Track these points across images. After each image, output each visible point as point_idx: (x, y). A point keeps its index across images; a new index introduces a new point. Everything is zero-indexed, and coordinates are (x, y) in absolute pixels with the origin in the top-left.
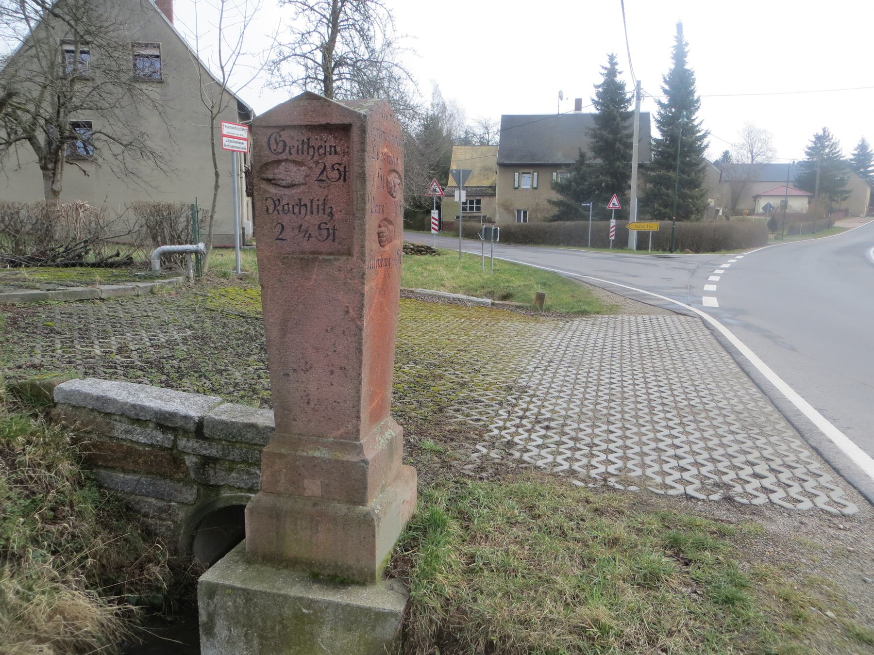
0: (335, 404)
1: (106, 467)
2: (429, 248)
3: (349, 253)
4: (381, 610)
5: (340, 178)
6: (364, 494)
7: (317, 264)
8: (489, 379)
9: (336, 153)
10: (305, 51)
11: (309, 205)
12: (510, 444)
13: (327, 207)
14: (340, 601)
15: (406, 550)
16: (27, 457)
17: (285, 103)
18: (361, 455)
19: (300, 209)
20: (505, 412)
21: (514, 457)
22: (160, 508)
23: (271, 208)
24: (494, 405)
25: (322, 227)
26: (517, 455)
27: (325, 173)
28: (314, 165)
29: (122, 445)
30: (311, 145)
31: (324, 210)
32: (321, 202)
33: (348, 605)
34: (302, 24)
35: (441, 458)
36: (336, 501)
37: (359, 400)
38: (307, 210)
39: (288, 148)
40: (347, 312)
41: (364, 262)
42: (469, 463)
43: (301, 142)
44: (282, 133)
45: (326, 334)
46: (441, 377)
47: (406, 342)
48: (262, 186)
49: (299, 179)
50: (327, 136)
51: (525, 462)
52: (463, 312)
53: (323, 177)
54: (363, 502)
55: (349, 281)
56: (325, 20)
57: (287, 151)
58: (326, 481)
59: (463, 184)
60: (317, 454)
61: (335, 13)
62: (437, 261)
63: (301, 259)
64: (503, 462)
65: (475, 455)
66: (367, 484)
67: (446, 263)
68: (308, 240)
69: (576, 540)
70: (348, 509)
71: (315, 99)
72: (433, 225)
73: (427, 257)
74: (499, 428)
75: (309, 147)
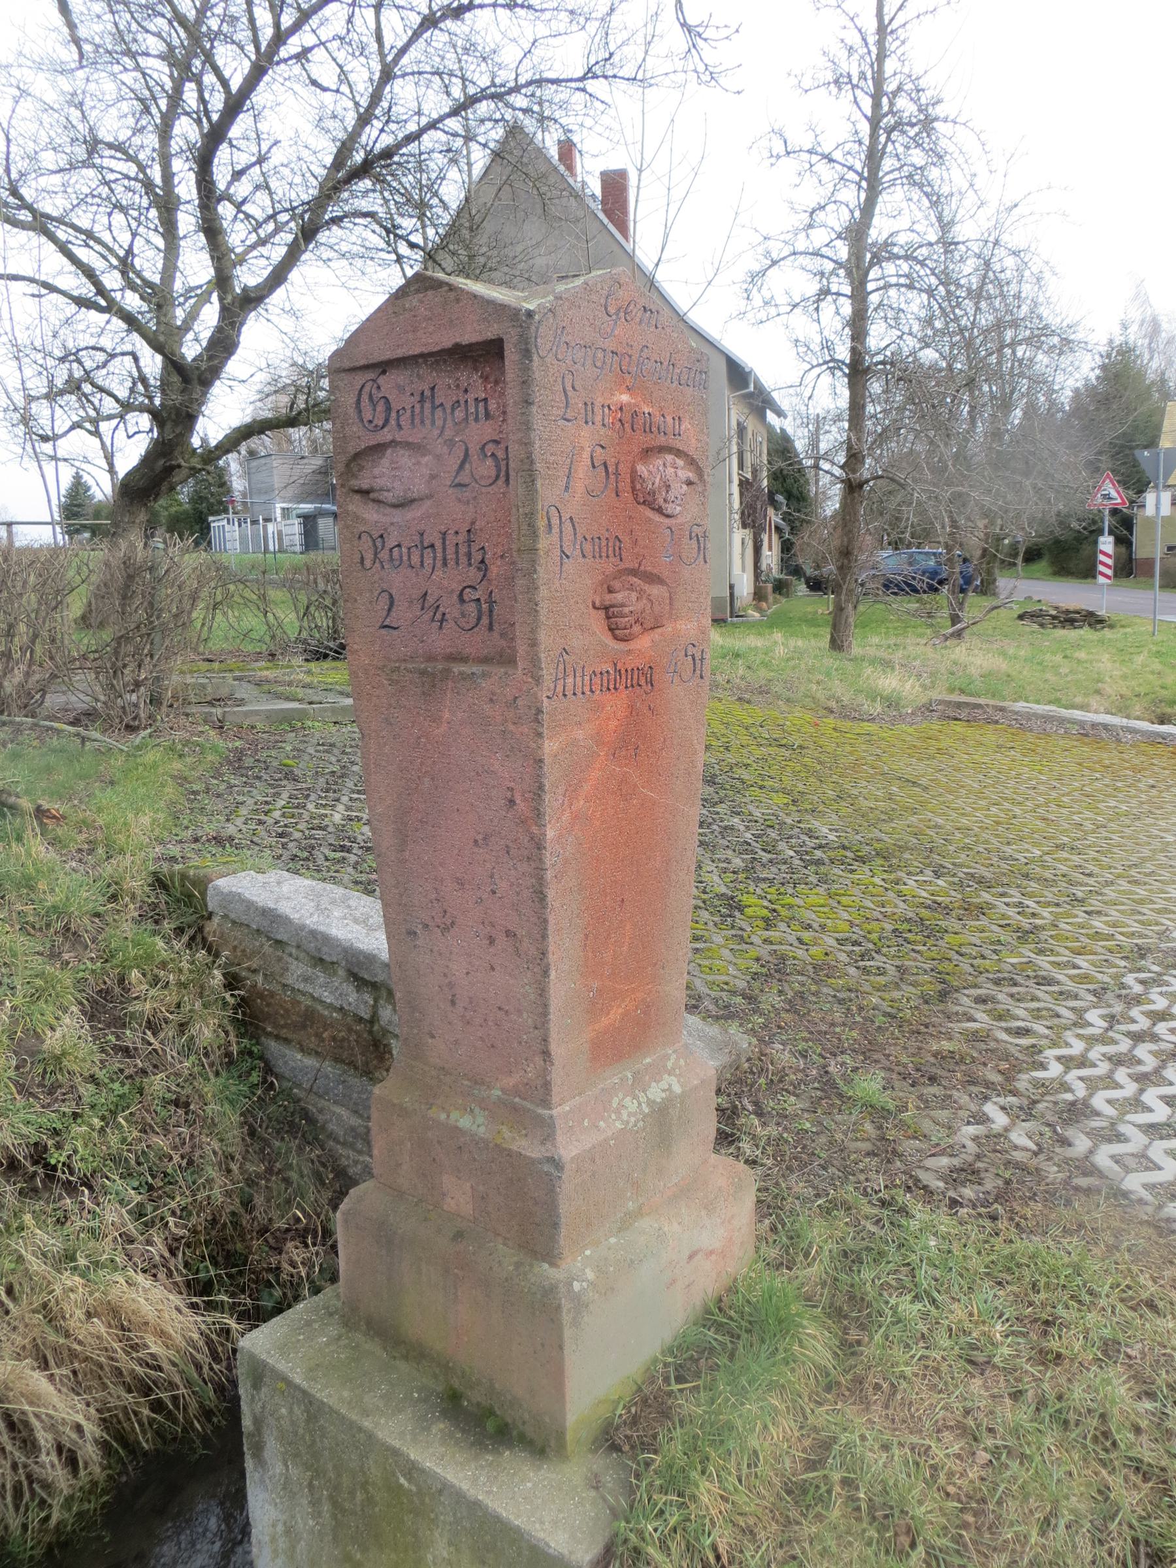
0: (500, 1014)
1: (277, 1037)
2: (1091, 614)
3: (511, 661)
4: (542, 1545)
5: (497, 477)
6: (553, 1238)
7: (450, 684)
8: (1098, 924)
9: (488, 416)
10: (817, 245)
11: (438, 545)
12: (1077, 1112)
13: (475, 547)
14: (465, 1486)
15: (680, 1379)
16: (148, 1006)
17: (379, 310)
18: (549, 1145)
19: (422, 556)
20: (1102, 1017)
21: (1070, 1152)
22: (353, 1129)
23: (369, 557)
24: (1082, 993)
25: (466, 597)
26: (1082, 1144)
27: (467, 466)
28: (445, 450)
29: (299, 1002)
30: (437, 403)
31: (469, 555)
32: (462, 538)
33: (476, 1504)
34: (811, 195)
35: (880, 1128)
36: (500, 1240)
37: (545, 1014)
38: (435, 558)
39: (394, 415)
40: (512, 802)
41: (538, 680)
42: (943, 1153)
43: (418, 398)
44: (381, 380)
45: (476, 850)
46: (982, 910)
47: (940, 821)
48: (351, 507)
49: (419, 487)
50: (469, 378)
51: (1091, 1170)
52: (1105, 756)
53: (464, 478)
54: (550, 1256)
55: (511, 727)
56: (851, 176)
57: (393, 422)
58: (481, 1188)
59: (1167, 477)
60: (465, 1122)
61: (874, 157)
62: (1101, 642)
63: (423, 673)
64: (1035, 1161)
65: (971, 1130)
66: (558, 1216)
67: (1120, 645)
68: (441, 628)
69: (1139, 1468)
70: (518, 1265)
71: (432, 288)
72: (1101, 568)
73: (1085, 633)
74: (1064, 1060)
75: (434, 408)
